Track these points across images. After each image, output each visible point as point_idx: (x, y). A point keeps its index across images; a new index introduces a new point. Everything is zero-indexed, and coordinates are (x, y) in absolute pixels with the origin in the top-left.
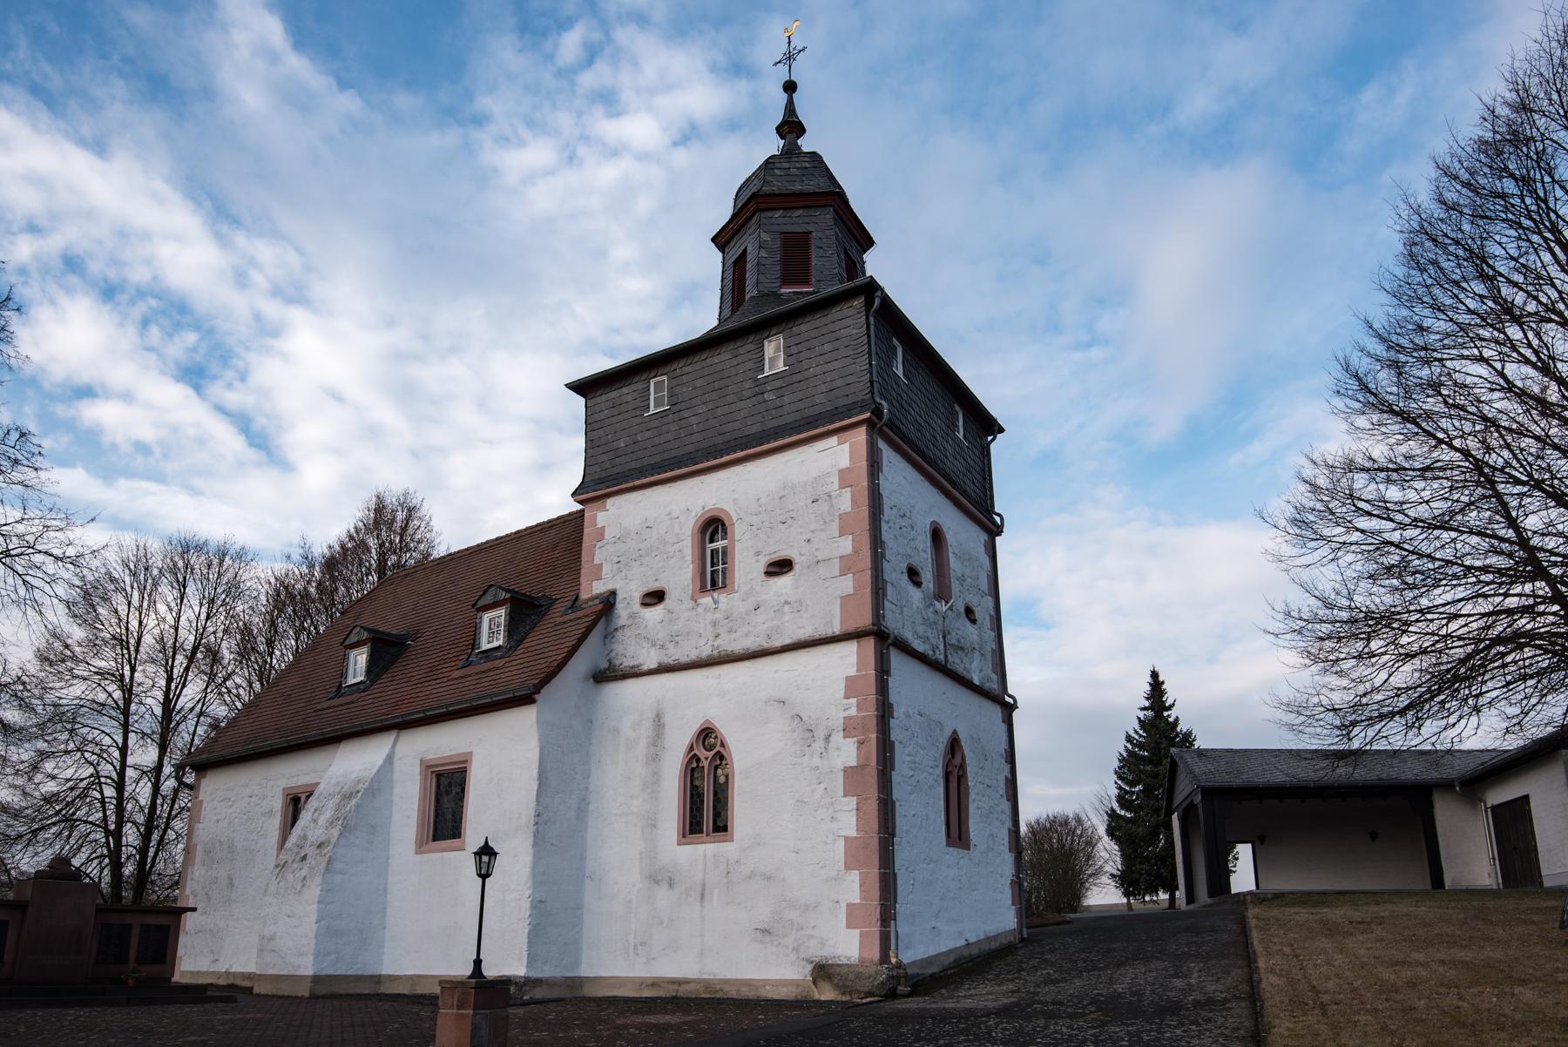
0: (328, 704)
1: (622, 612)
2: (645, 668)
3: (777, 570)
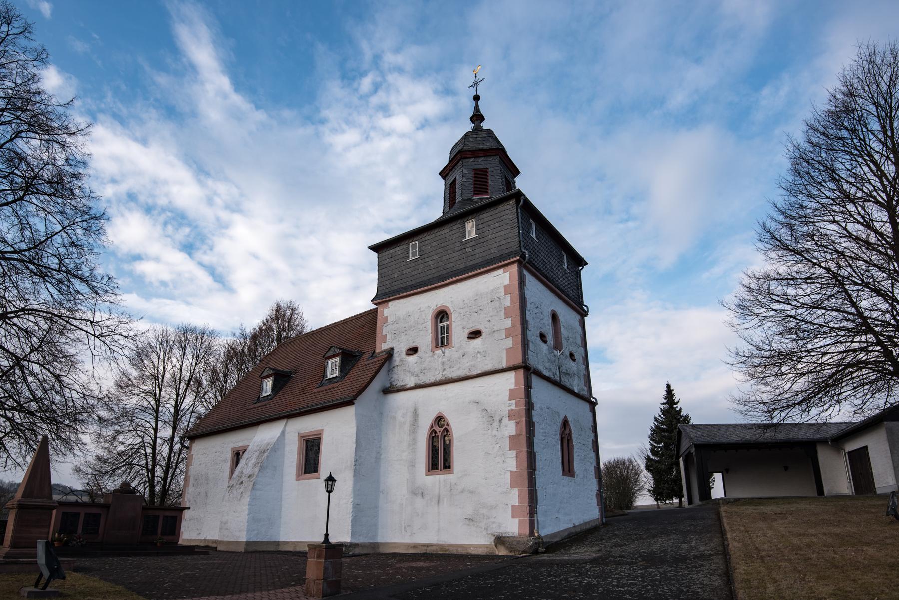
0: (253, 406)
1: (396, 358)
2: (408, 386)
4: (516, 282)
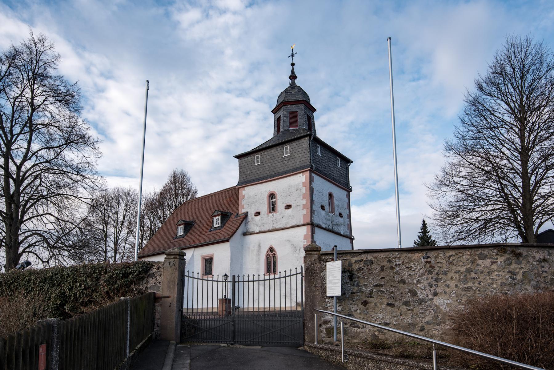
0: (174, 241)
1: (250, 217)
2: (256, 232)
3: (288, 207)
4: (308, 181)
